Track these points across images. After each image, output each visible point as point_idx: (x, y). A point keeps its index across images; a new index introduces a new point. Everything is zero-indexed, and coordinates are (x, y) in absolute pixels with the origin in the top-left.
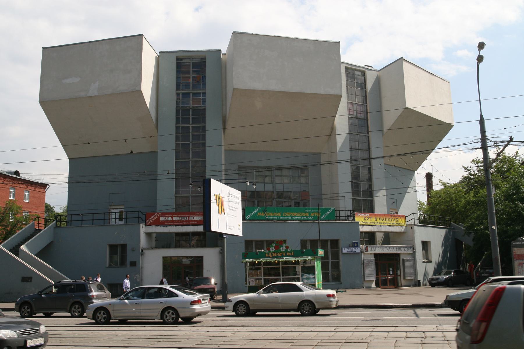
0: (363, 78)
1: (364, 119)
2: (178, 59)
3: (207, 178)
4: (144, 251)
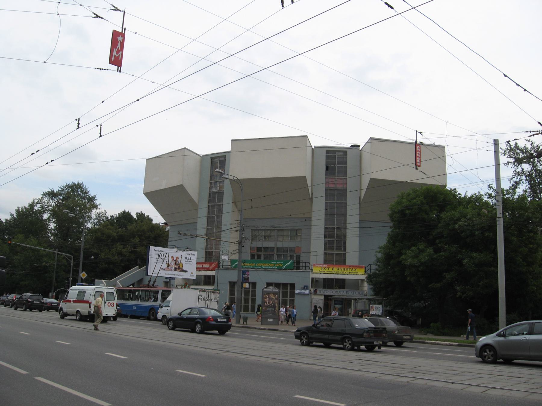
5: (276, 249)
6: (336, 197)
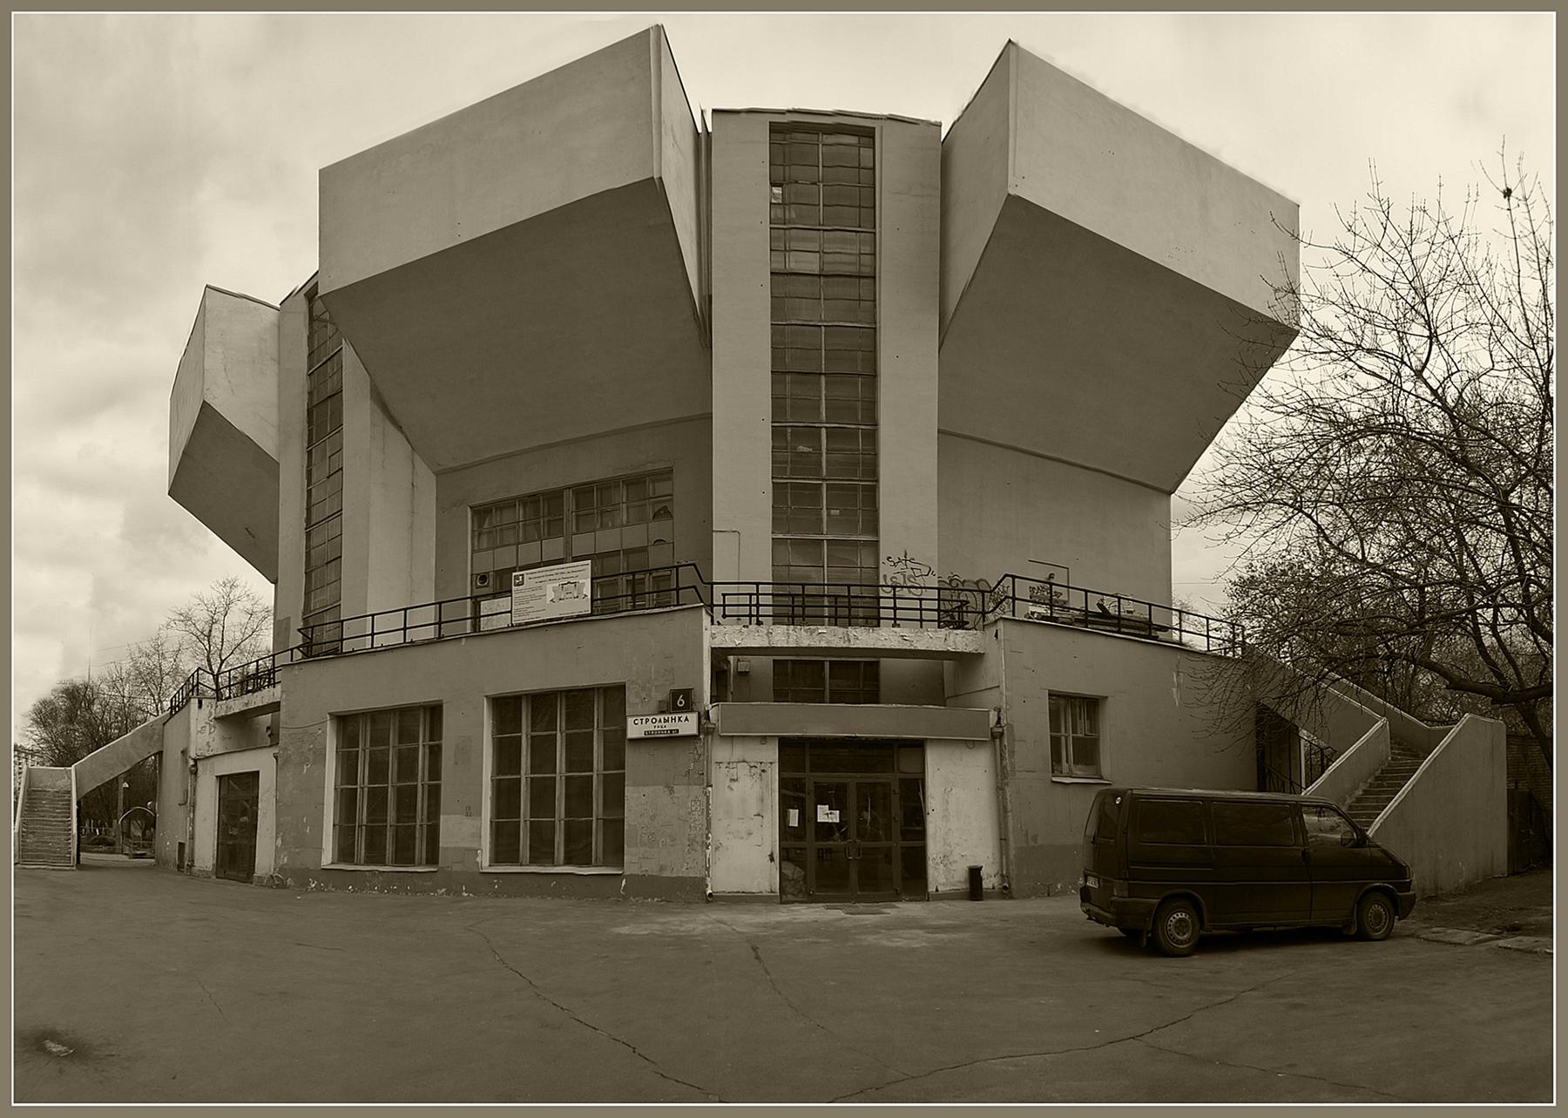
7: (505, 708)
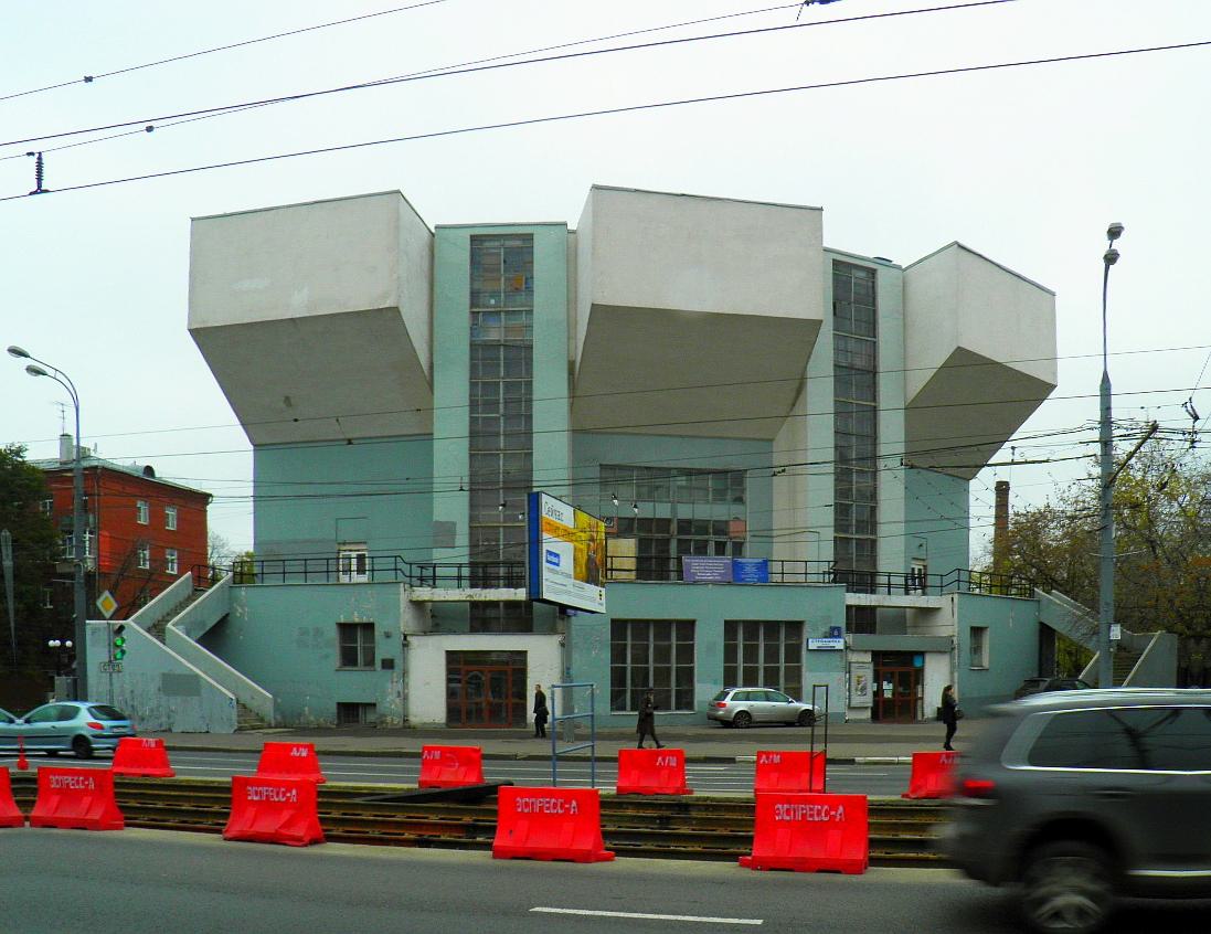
0: (870, 284)
1: (869, 372)
2: (473, 238)
3: (535, 490)
4: (408, 638)
5: (674, 527)
6: (500, 370)
7: (730, 627)
